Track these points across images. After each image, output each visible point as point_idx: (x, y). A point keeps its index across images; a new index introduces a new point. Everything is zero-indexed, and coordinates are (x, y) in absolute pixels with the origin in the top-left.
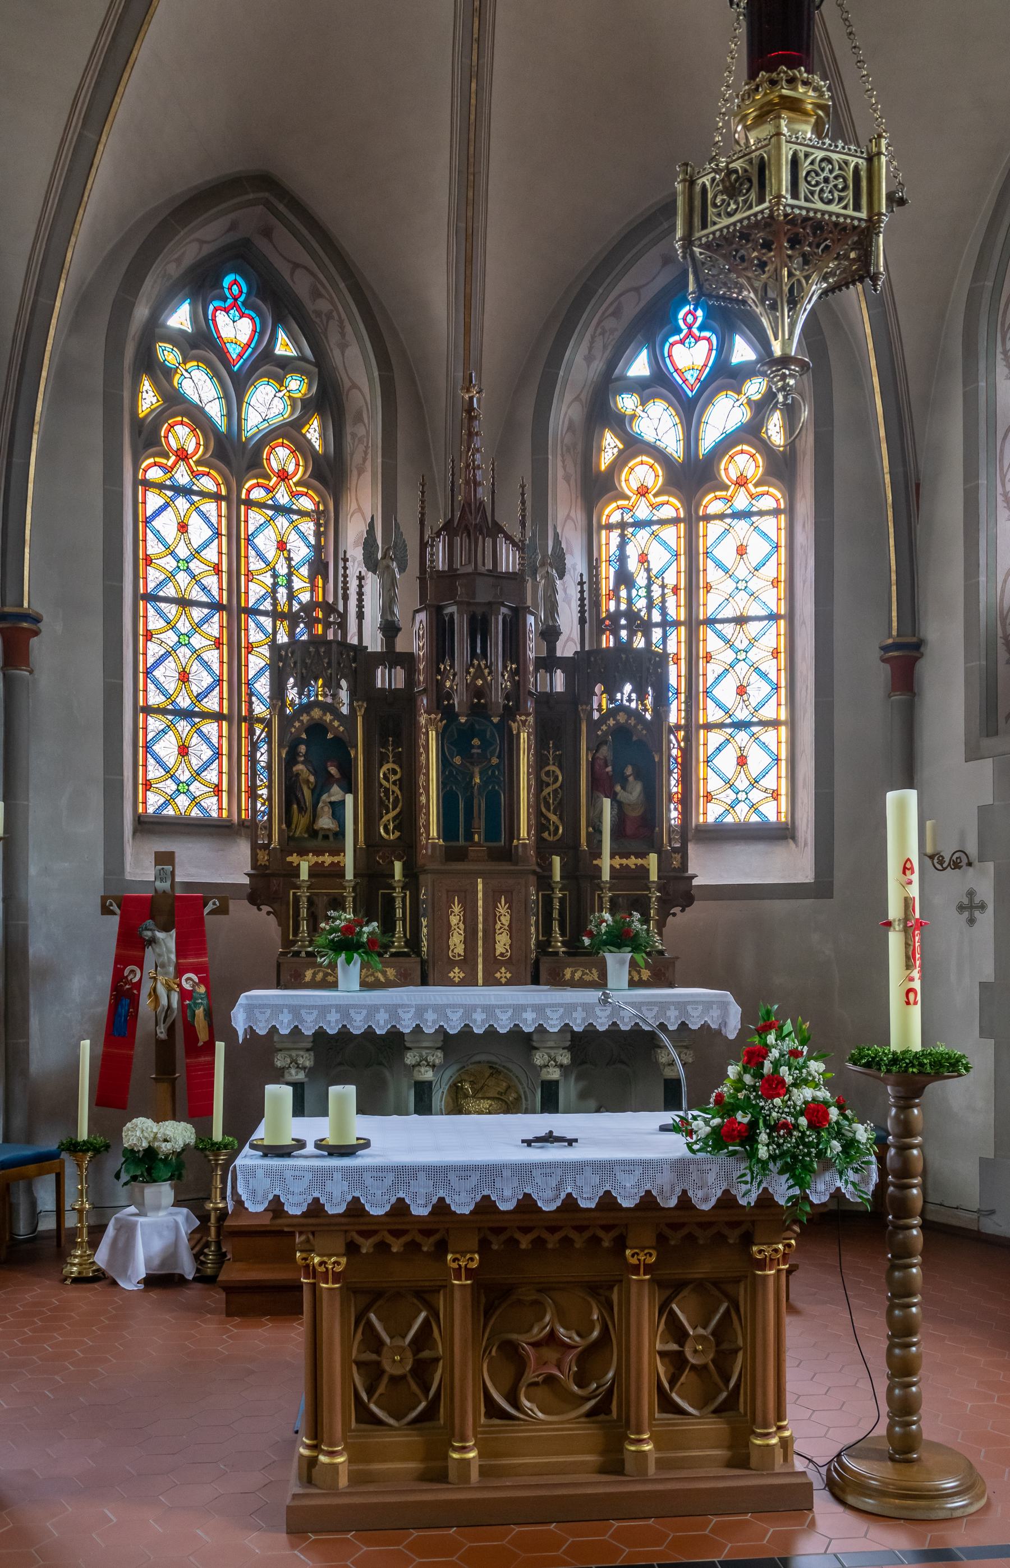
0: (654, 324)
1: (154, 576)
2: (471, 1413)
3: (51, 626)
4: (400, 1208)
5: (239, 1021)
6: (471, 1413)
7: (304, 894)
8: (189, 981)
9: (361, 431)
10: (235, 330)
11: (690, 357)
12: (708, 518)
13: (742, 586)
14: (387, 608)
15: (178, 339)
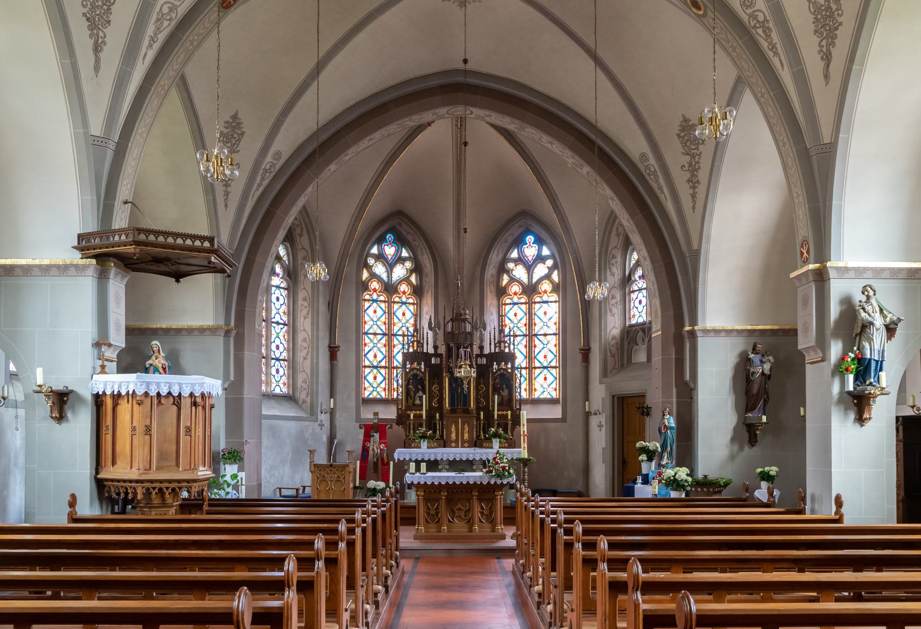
0: (519, 242)
1: (367, 327)
2: (445, 521)
4: (433, 483)
5: (396, 456)
6: (445, 521)
7: (412, 423)
9: (428, 280)
10: (390, 251)
11: (530, 251)
12: (535, 303)
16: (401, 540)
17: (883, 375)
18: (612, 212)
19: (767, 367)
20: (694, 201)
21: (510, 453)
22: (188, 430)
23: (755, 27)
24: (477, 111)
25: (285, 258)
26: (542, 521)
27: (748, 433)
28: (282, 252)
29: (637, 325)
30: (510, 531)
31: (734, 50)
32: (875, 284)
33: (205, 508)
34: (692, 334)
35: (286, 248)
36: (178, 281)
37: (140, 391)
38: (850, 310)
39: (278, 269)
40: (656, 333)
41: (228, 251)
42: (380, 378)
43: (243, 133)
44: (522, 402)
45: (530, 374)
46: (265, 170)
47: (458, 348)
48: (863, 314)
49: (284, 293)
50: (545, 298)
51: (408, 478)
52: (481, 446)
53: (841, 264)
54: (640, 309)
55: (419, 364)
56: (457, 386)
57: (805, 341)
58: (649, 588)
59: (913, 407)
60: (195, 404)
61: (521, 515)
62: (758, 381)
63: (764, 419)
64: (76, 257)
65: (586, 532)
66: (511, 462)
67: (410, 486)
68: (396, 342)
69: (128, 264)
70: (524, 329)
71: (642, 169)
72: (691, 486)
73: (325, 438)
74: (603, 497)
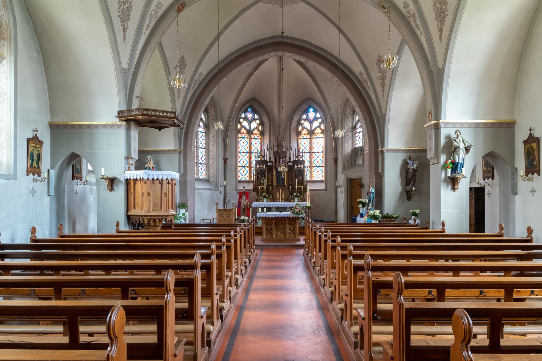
0: (306, 111)
1: (240, 149)
3: (229, 159)
5: (253, 206)
6: (274, 233)
8: (247, 201)
10: (250, 116)
11: (311, 115)
13: (318, 148)
14: (270, 155)
15: (243, 118)
16: (255, 241)
17: (463, 169)
18: (347, 98)
19: (415, 166)
20: (383, 93)
21: (302, 204)
22: (166, 194)
23: (409, 17)
24: (288, 54)
25: (204, 120)
26: (315, 232)
27: (407, 195)
28: (203, 117)
29: (358, 148)
30: (302, 238)
31: (400, 27)
32: (461, 130)
33: (173, 227)
34: (382, 152)
35: (205, 115)
36: (160, 131)
37: (145, 178)
38: (449, 141)
39: (201, 124)
40: (366, 151)
41: (181, 118)
42: (246, 172)
43: (186, 65)
44: (307, 182)
45: (311, 170)
46: (196, 81)
47: (280, 158)
48: (455, 143)
49: (204, 134)
50: (318, 136)
51: (258, 215)
52: (290, 201)
53: (446, 121)
54: (359, 142)
55: (263, 165)
56: (279, 175)
57: (430, 155)
58: (375, 269)
59: (478, 183)
60: (168, 183)
61: (307, 231)
62: (411, 172)
63: (414, 189)
64: (117, 121)
65: (342, 241)
66: (303, 208)
67: (259, 218)
68: (252, 156)
69: (139, 123)
70: (308, 150)
71: (360, 78)
72: (381, 218)
73: (222, 198)
74: (343, 222)
